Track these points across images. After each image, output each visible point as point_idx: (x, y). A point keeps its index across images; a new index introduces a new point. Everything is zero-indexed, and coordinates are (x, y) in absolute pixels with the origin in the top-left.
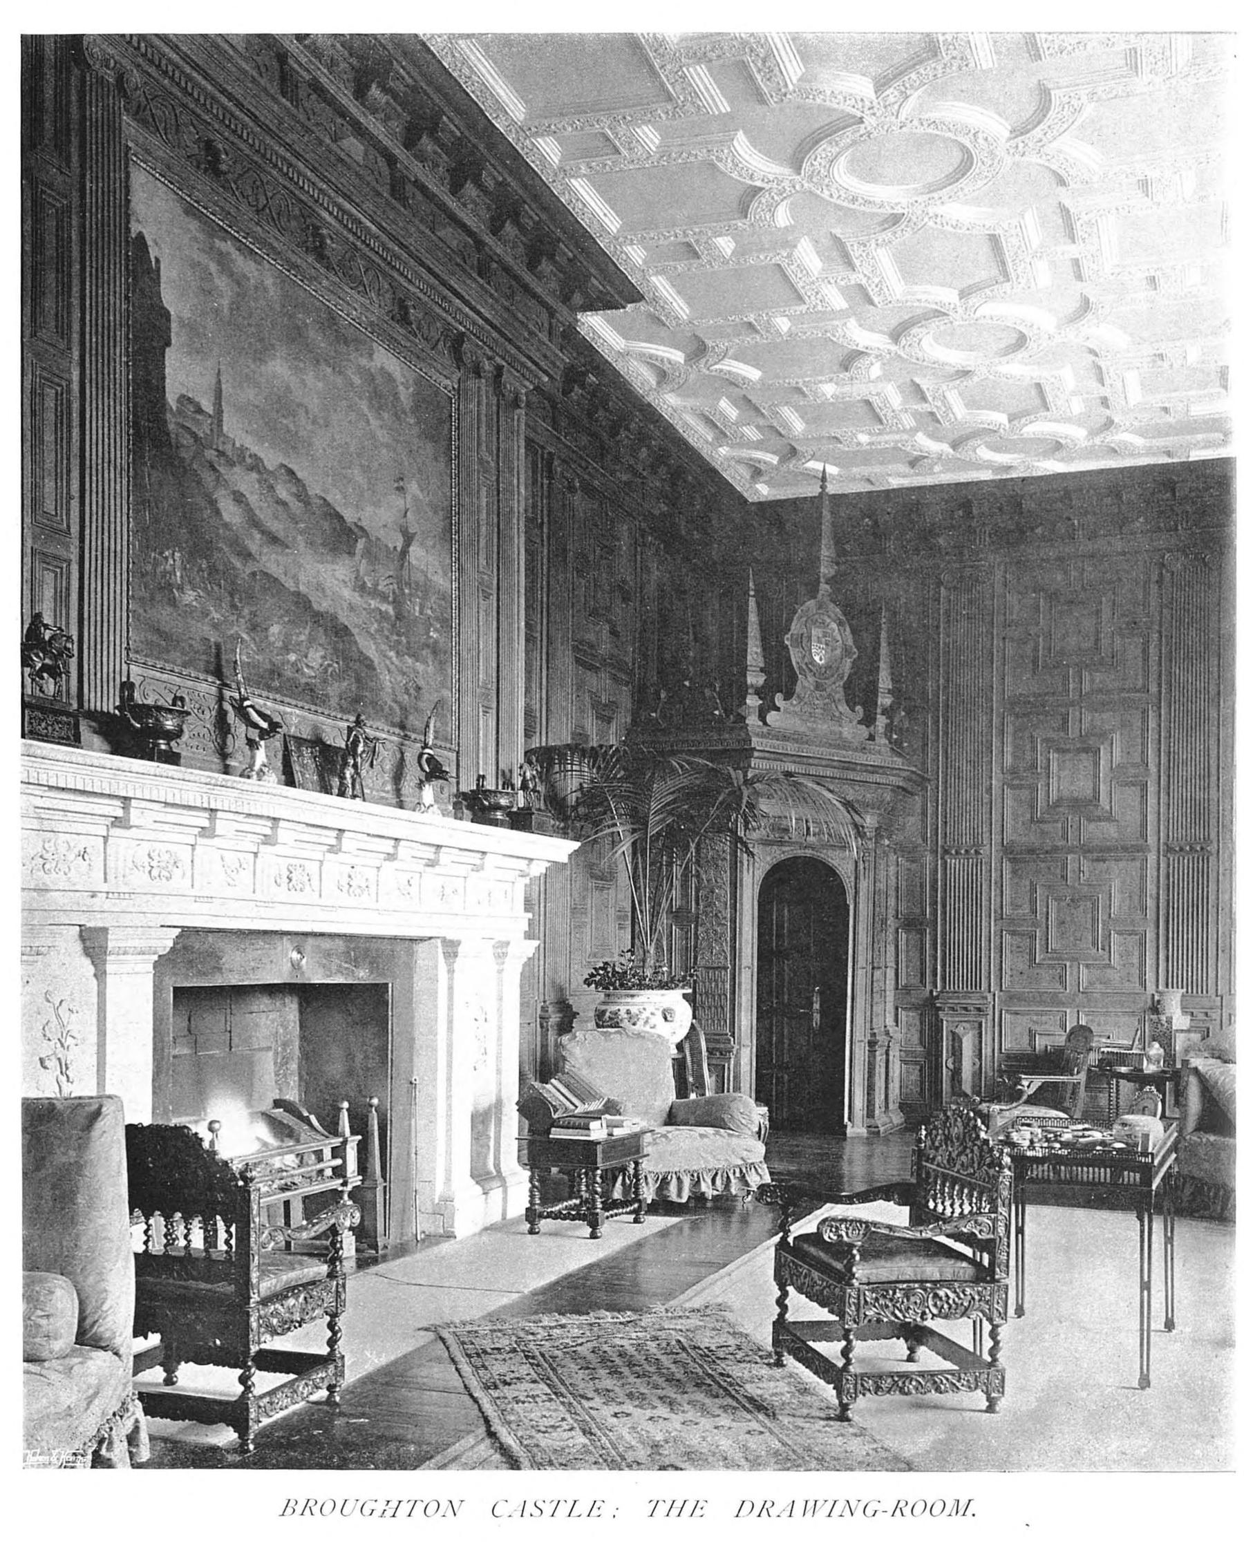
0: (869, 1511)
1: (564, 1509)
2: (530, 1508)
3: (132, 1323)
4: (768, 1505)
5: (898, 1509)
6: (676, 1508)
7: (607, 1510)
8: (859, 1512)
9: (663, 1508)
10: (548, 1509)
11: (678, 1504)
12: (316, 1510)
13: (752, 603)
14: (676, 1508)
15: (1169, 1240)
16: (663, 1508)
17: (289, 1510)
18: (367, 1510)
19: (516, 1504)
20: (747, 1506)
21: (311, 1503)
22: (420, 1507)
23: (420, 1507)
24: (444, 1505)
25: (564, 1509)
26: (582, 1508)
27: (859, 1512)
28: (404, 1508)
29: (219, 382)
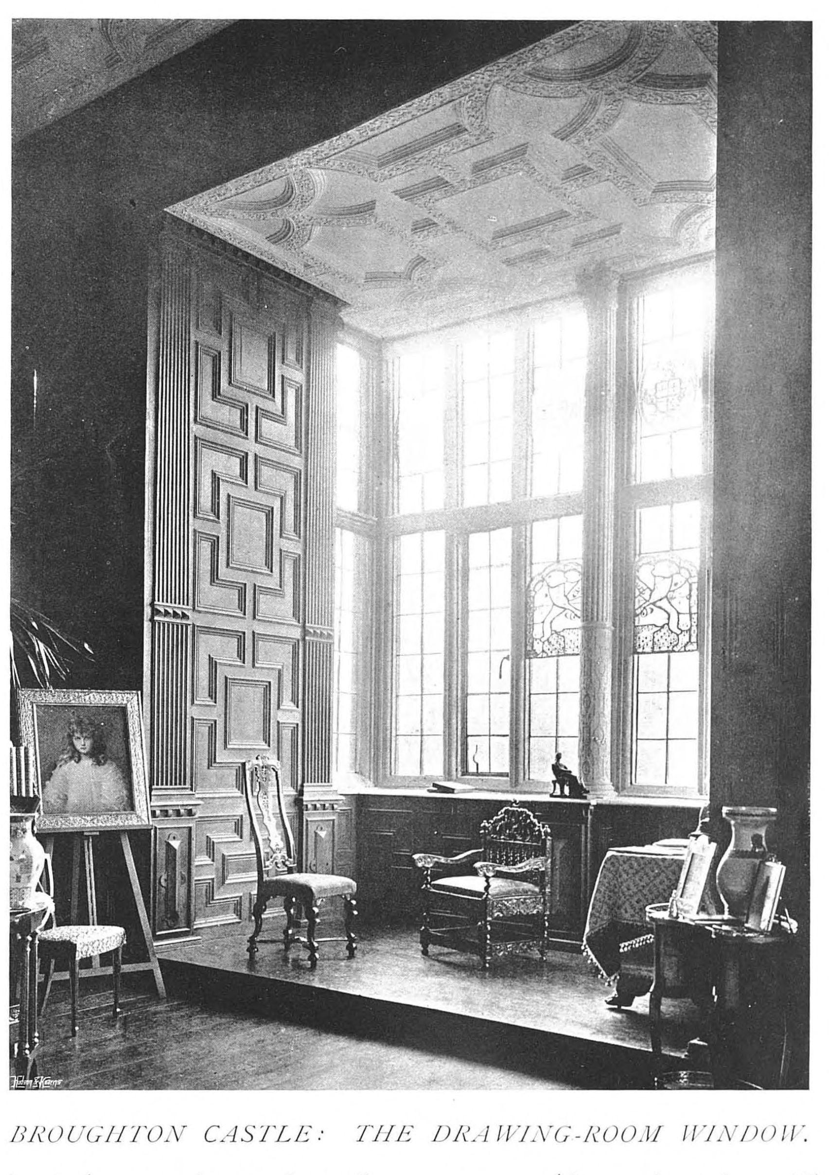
0: (561, 1137)
1: (273, 1134)
2: (241, 1134)
3: (546, 1030)
4: (464, 1129)
5: (591, 1135)
6: (384, 1134)
7: (313, 1134)
8: (550, 1138)
9: (371, 1134)
10: (258, 1134)
11: (386, 1129)
12: (44, 1137)
13: (721, 896)
14: (384, 1134)
15: (341, 534)
16: (371, 1134)
17: (19, 1137)
18: (93, 1137)
19: (227, 1128)
20: (444, 1132)
21: (595, 1130)
22: (143, 1133)
23: (143, 1133)
24: (167, 1130)
25: (273, 1134)
26: (291, 1133)
27: (550, 1138)
28: (129, 1134)
29: (510, 309)
